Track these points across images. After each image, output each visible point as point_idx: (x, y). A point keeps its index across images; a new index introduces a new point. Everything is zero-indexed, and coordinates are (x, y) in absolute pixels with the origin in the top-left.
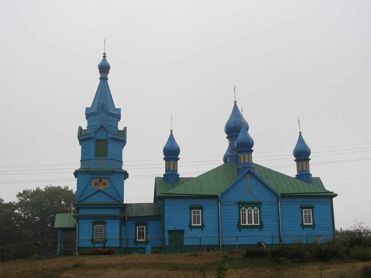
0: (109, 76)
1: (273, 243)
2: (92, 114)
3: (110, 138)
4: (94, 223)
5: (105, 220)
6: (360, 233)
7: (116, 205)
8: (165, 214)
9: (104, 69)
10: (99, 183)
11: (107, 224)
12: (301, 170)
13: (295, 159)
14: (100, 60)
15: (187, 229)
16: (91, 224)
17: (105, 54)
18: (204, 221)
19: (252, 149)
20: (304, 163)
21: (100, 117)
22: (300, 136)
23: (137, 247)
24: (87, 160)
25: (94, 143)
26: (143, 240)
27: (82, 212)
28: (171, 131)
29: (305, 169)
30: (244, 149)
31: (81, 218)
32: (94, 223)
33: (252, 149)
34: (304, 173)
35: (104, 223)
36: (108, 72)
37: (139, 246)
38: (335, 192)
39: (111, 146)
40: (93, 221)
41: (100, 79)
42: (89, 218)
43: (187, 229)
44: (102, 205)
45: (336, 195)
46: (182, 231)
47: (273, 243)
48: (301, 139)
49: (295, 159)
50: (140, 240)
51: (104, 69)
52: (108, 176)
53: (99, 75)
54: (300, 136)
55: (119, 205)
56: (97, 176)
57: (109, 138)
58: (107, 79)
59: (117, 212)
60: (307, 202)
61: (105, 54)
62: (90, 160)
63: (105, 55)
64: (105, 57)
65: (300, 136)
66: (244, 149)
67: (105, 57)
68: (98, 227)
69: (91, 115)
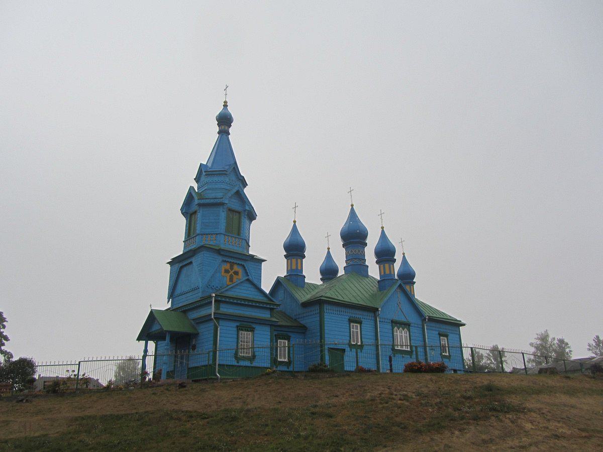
1: (293, 370)
2: (218, 173)
4: (239, 328)
5: (254, 326)
6: (410, 364)
7: (267, 304)
8: (325, 325)
9: (225, 121)
10: (233, 271)
11: (256, 332)
12: (389, 273)
13: (285, 254)
14: (220, 109)
15: (348, 349)
16: (235, 329)
17: (226, 102)
18: (363, 340)
22: (383, 232)
23: (240, 364)
24: (212, 234)
25: (225, 212)
26: (285, 360)
27: (225, 309)
31: (223, 319)
32: (239, 328)
34: (386, 278)
35: (252, 330)
37: (242, 363)
39: (245, 221)
40: (238, 324)
41: (219, 133)
42: (230, 319)
43: (348, 349)
46: (344, 350)
47: (293, 370)
48: (295, 230)
49: (285, 254)
50: (281, 360)
51: (225, 121)
52: (242, 263)
54: (383, 232)
55: (270, 304)
56: (230, 260)
57: (245, 211)
58: (229, 134)
59: (265, 315)
60: (358, 314)
61: (226, 102)
62: (218, 235)
64: (225, 106)
65: (383, 232)
67: (225, 106)
68: (244, 334)
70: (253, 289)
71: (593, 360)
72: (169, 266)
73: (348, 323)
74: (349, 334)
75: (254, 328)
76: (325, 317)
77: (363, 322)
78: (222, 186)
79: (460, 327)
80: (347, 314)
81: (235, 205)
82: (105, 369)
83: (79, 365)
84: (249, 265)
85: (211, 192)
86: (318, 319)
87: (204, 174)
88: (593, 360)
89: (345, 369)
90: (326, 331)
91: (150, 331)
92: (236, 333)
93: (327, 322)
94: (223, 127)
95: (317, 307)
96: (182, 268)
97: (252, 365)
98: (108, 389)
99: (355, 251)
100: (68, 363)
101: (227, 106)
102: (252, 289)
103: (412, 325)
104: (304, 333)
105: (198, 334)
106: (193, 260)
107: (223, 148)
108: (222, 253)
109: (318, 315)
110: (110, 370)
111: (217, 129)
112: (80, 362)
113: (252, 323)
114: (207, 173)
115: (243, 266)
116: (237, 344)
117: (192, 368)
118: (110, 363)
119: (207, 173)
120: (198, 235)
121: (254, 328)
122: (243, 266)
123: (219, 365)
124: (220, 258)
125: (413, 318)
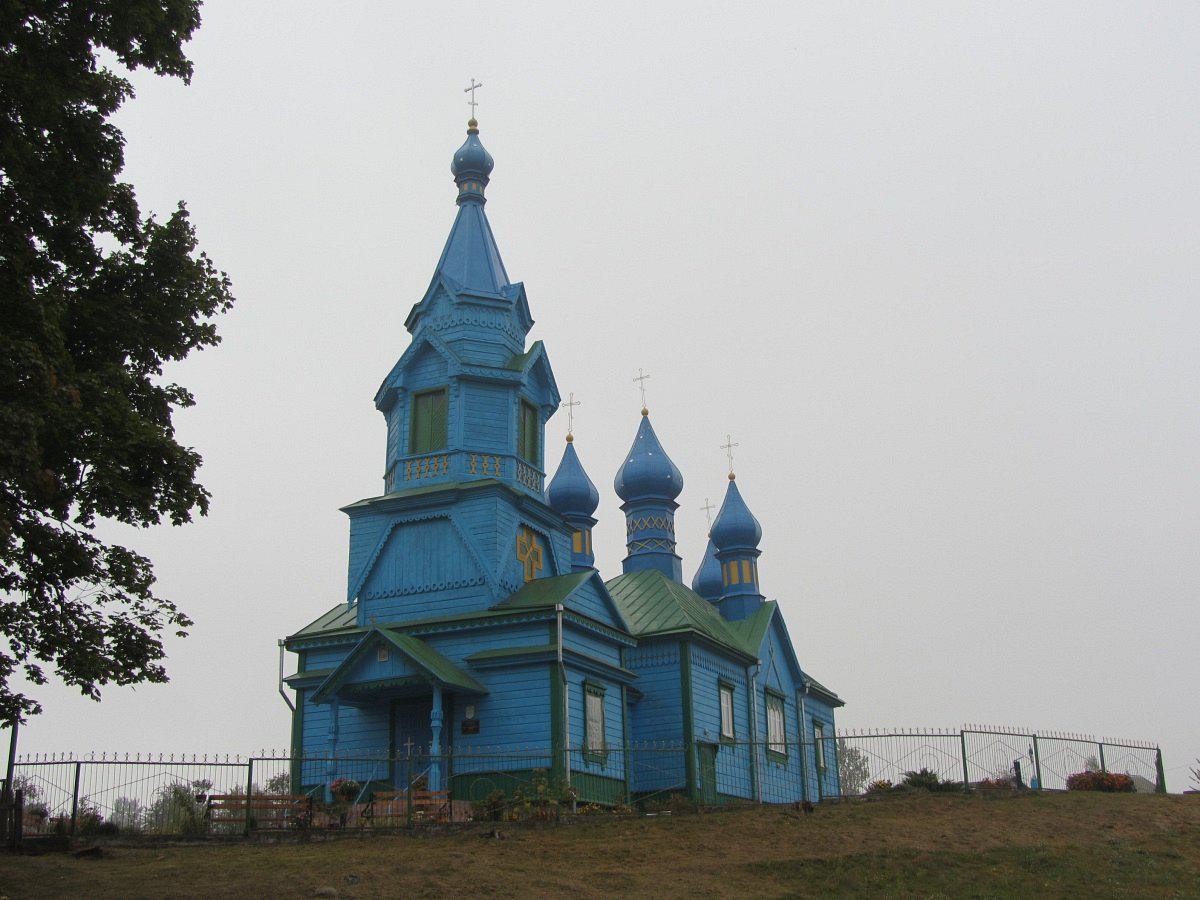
0: (489, 192)
3: (455, 379)
5: (604, 684)
9: (472, 170)
14: (460, 139)
17: (473, 123)
19: (676, 500)
20: (745, 564)
21: (435, 320)
24: (492, 456)
28: (732, 477)
29: (747, 579)
30: (740, 546)
33: (676, 500)
36: (485, 181)
38: (840, 697)
44: (471, 621)
45: (840, 704)
51: (472, 170)
53: (455, 192)
54: (732, 487)
58: (482, 201)
61: (473, 123)
63: (473, 127)
64: (473, 132)
65: (732, 487)
66: (740, 546)
67: (473, 132)
69: (485, 306)
72: (346, 517)
73: (716, 688)
77: (736, 689)
78: (498, 337)
81: (529, 392)
82: (918, 756)
83: (250, 765)
85: (474, 348)
86: (678, 674)
87: (512, 307)
91: (357, 680)
92: (580, 699)
93: (697, 680)
94: (466, 187)
95: (675, 649)
96: (397, 527)
97: (605, 774)
99: (651, 521)
100: (153, 760)
101: (477, 132)
102: (595, 599)
105: (487, 694)
106: (454, 513)
108: (524, 505)
109: (677, 667)
111: (455, 192)
112: (251, 760)
113: (604, 677)
114: (465, 299)
115: (544, 539)
116: (798, 723)
117: (461, 776)
119: (465, 299)
120: (457, 452)
122: (544, 539)
123: (571, 771)
124: (518, 518)
125: (787, 689)
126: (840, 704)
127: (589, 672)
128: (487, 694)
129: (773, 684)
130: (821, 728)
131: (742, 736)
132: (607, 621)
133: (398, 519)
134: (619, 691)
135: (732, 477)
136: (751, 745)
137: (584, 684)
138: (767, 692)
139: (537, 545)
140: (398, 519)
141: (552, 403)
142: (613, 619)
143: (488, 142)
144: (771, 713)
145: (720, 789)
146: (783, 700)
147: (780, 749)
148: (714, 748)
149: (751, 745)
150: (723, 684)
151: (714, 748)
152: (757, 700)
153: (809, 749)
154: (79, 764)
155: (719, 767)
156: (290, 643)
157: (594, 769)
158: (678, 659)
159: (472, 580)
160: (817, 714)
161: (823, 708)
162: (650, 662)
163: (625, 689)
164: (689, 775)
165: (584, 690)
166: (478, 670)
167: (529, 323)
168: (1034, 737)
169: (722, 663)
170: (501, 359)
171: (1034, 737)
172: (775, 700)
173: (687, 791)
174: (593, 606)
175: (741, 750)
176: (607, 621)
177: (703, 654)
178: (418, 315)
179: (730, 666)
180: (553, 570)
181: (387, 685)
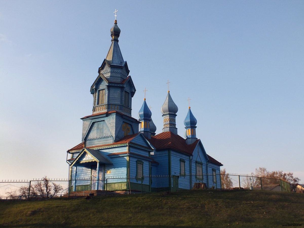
3: (107, 86)
5: (143, 161)
14: (112, 26)
16: (135, 163)
45: (222, 165)
51: (116, 33)
54: (190, 110)
61: (116, 21)
67: (116, 23)
70: (142, 140)
71: (117, 192)
73: (179, 162)
74: (143, 167)
75: (143, 163)
76: (171, 158)
79: (220, 167)
80: (165, 155)
84: (133, 125)
86: (168, 158)
88: (117, 192)
89: (179, 188)
90: (172, 166)
95: (167, 152)
98: (125, 195)
103: (203, 164)
104: (157, 166)
107: (116, 50)
109: (168, 156)
110: (9, 189)
112: (30, 181)
115: (131, 125)
118: (111, 180)
121: (143, 163)
122: (131, 125)
125: (203, 161)
126: (222, 165)
127: (138, 158)
128: (112, 164)
129: (199, 160)
130: (215, 171)
131: (187, 173)
132: (145, 145)
133: (93, 121)
134: (148, 163)
135: (145, 99)
136: (191, 176)
137: (137, 161)
138: (196, 162)
139: (129, 127)
140: (93, 121)
141: (133, 91)
142: (147, 145)
143: (119, 26)
144: (198, 168)
145: (179, 187)
146: (202, 165)
147: (201, 177)
148: (178, 177)
149: (191, 176)
150: (182, 161)
151: (178, 177)
152: (193, 165)
153: (214, 177)
154: (216, 174)
155: (179, 182)
156: (68, 152)
157: (140, 182)
158: (168, 155)
159: (110, 136)
160: (214, 168)
161: (216, 166)
162: (161, 155)
163: (150, 162)
164: (170, 185)
165: (137, 163)
166: (111, 158)
167: (128, 72)
168: (239, 176)
169: (181, 155)
170: (120, 80)
171: (239, 176)
172: (199, 165)
173: (169, 189)
174: (141, 142)
175: (188, 177)
176: (145, 145)
177: (175, 153)
178: (100, 70)
179: (184, 156)
180: (134, 133)
181: (90, 161)
